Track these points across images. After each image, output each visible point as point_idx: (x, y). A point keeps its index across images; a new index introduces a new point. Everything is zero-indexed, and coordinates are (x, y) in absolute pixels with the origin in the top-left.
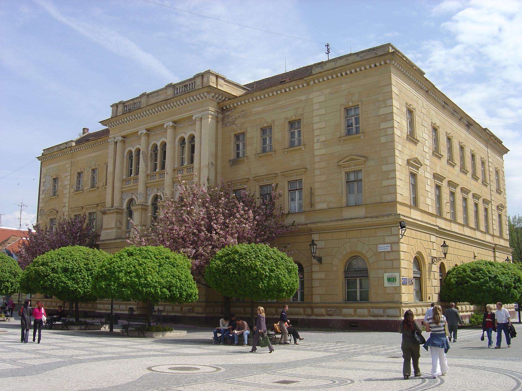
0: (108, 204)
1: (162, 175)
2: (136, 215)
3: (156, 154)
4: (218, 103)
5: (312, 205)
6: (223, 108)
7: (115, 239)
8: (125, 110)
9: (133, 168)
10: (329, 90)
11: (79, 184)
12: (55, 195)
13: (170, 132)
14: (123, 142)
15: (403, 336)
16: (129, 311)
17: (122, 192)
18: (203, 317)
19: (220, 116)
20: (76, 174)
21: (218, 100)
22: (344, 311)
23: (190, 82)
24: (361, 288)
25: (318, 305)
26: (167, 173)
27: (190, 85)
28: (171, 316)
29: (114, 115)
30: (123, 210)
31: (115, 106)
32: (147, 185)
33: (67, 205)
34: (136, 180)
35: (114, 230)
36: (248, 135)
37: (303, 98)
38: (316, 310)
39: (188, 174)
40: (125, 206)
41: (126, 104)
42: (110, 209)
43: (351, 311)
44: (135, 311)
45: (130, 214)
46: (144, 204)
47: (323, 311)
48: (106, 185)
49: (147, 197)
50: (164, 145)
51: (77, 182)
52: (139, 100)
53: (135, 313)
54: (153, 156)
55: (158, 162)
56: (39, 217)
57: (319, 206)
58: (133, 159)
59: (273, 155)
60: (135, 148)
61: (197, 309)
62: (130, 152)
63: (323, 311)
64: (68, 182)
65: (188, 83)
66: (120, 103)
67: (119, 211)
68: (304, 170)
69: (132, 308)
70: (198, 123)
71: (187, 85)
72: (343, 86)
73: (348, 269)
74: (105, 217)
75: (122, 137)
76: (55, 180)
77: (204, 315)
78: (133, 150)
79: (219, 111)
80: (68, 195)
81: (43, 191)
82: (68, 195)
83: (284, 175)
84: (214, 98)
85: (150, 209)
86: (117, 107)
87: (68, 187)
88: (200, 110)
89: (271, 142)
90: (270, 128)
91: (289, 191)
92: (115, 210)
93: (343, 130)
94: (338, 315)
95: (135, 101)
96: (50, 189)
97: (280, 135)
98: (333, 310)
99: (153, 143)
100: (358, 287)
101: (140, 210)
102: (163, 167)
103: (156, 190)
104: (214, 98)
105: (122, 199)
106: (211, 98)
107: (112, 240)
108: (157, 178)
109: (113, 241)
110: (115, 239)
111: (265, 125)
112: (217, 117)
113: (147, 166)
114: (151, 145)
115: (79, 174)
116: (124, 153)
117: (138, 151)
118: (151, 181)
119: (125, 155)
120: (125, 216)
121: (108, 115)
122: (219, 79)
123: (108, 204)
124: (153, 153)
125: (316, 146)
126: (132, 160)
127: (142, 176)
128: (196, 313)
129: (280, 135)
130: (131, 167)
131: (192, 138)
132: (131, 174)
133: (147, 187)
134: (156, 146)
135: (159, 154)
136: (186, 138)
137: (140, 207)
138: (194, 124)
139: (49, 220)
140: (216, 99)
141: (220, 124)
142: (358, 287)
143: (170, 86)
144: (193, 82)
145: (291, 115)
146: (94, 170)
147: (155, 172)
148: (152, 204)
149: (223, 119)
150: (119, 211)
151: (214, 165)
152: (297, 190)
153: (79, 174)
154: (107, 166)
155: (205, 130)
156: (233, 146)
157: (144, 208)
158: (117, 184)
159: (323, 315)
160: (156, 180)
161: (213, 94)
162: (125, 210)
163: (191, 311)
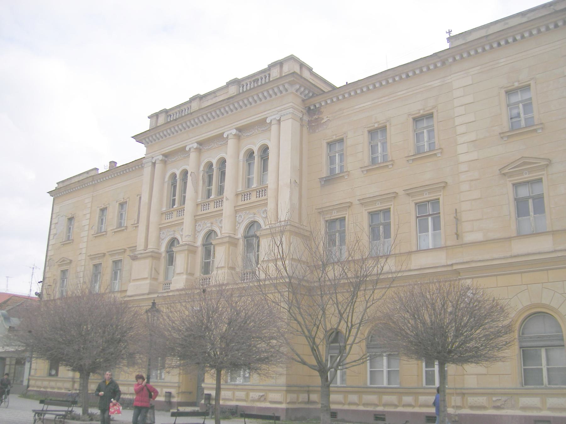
0: (141, 247)
1: (219, 202)
2: (180, 261)
3: (210, 177)
4: (303, 101)
5: (457, 235)
6: (309, 108)
7: (148, 294)
8: (166, 126)
9: (177, 198)
10: (479, 68)
11: (102, 224)
12: (69, 240)
13: (231, 143)
14: (164, 162)
15: (28, 298)
16: (166, 396)
17: (161, 229)
18: (282, 409)
19: (306, 118)
20: (98, 211)
21: (303, 96)
22: (525, 401)
23: (263, 75)
24: (548, 364)
25: (476, 391)
26: (227, 199)
27: (262, 79)
28: (231, 406)
29: (154, 126)
30: (160, 254)
31: (155, 116)
32: (196, 218)
33: (84, 251)
34: (181, 211)
35: (148, 281)
36: (349, 142)
37: (437, 83)
38: (471, 400)
39: (258, 199)
40: (163, 249)
41: (169, 114)
42: (142, 252)
43: (535, 401)
44: (174, 397)
45: (171, 260)
46: (192, 244)
47: (482, 400)
48: (138, 223)
49: (195, 234)
50: (223, 162)
51: (99, 222)
52: (188, 105)
53: (175, 400)
54: (207, 180)
55: (214, 187)
56: (47, 268)
57: (469, 238)
58: (178, 184)
59: (390, 167)
60: (180, 170)
61: (272, 396)
62: (174, 176)
63: (482, 400)
64: (87, 222)
65: (259, 77)
66: (161, 112)
67: (155, 256)
68: (443, 185)
69: (170, 393)
70: (274, 128)
71: (258, 80)
72: (502, 60)
73: (523, 334)
74: (136, 264)
75: (163, 155)
76: (71, 219)
77: (284, 406)
78: (178, 173)
79: (304, 111)
80: (85, 239)
81: (55, 234)
82: (86, 238)
83: (408, 194)
84: (298, 93)
85: (200, 252)
86: (157, 118)
87: (86, 228)
88: (279, 108)
89: (384, 149)
90: (383, 129)
91: (417, 217)
92: (150, 254)
93: (506, 125)
94: (513, 407)
95: (182, 108)
96: (64, 231)
97: (400, 139)
98: (504, 398)
99: (206, 161)
100: (544, 362)
101: (186, 252)
102: (221, 190)
103: (209, 225)
104: (298, 93)
105: (159, 239)
106: (294, 91)
107: (143, 294)
108: (212, 208)
109: (146, 297)
110: (148, 294)
111: (376, 125)
112: (301, 119)
113: (196, 192)
114: (203, 164)
115: (103, 210)
116: (164, 178)
117: (185, 173)
118: (203, 212)
119: (166, 179)
120: (163, 262)
121: (145, 126)
122: (303, 68)
123: (141, 247)
124: (206, 175)
125: (461, 149)
126: (175, 187)
127: (189, 205)
128: (271, 402)
129: (400, 139)
130: (174, 195)
131: (265, 150)
132: (174, 204)
133: (196, 221)
134: (210, 165)
135: (214, 174)
136: (256, 149)
137: (186, 247)
138: (269, 130)
139: (59, 272)
140: (301, 94)
141: (305, 130)
142: (544, 362)
143: (235, 82)
144: (267, 74)
145: (417, 108)
146: (122, 205)
147: (209, 200)
148: (204, 245)
149: (310, 122)
150: (155, 256)
151: (298, 184)
152: (429, 215)
153: (103, 210)
154: (140, 198)
155: (284, 140)
156: (324, 159)
157: (192, 250)
158: (154, 218)
159: (484, 408)
160: (209, 211)
161: (298, 87)
162: (164, 255)
163: (262, 399)
